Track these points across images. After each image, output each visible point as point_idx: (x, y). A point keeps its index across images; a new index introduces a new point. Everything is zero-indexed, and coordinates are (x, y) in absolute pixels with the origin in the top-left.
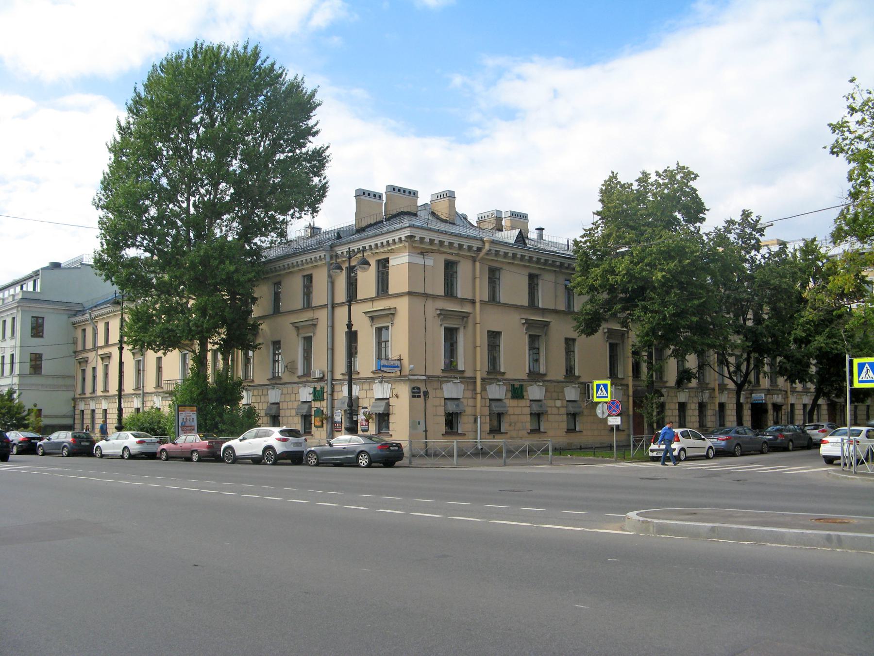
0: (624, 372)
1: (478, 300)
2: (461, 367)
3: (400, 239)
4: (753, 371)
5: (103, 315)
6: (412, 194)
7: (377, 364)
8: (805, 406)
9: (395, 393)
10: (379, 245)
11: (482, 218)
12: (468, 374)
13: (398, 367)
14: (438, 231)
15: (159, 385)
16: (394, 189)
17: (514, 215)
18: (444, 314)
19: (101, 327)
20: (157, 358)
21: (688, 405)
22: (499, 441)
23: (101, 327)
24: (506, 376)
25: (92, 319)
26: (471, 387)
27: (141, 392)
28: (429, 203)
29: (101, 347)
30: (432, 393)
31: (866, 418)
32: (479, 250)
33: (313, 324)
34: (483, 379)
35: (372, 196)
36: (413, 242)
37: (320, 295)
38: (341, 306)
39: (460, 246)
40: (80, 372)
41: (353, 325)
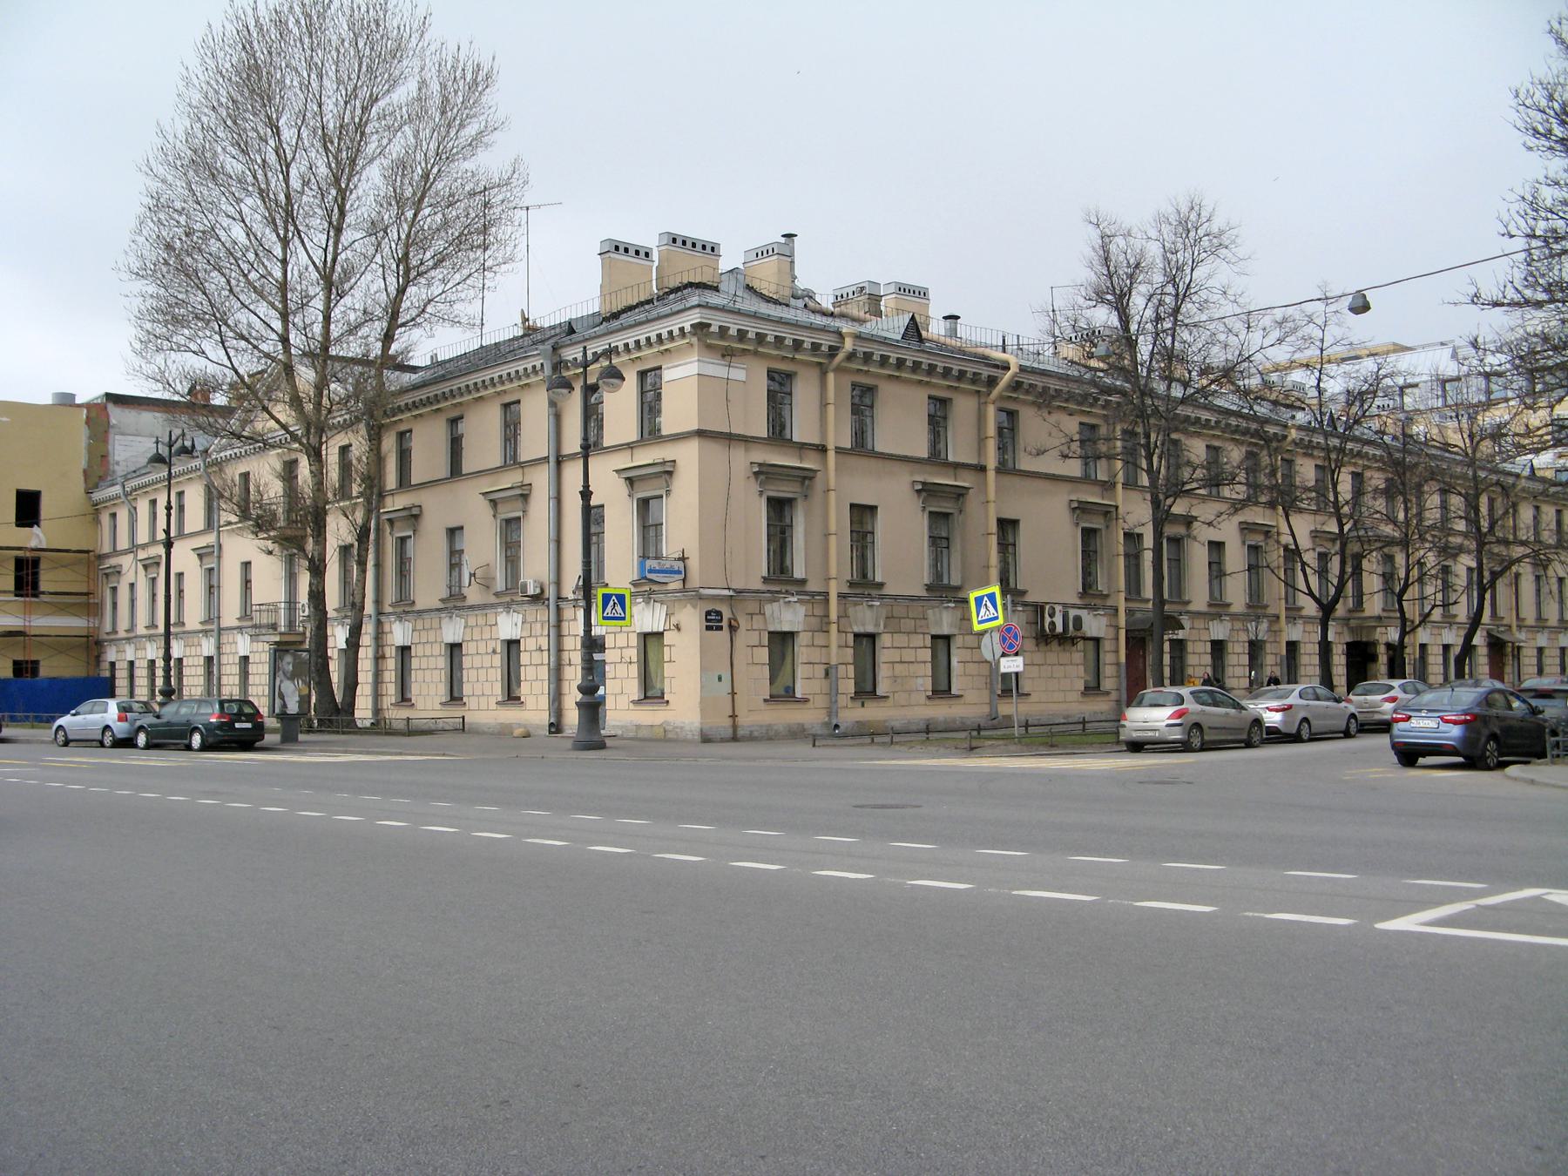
0: (1111, 578)
1: (831, 446)
2: (799, 573)
3: (682, 329)
4: (1350, 581)
5: (146, 486)
6: (708, 250)
7: (642, 566)
8: (1446, 648)
9: (674, 620)
10: (643, 342)
11: (842, 296)
12: (812, 586)
13: (679, 572)
14: (755, 316)
15: (246, 614)
16: (674, 240)
17: (903, 290)
18: (764, 473)
19: (143, 507)
20: (242, 563)
21: (1230, 645)
22: (871, 713)
23: (143, 507)
24: (886, 591)
25: (126, 495)
26: (818, 611)
27: (214, 627)
28: (741, 267)
29: (144, 546)
30: (743, 622)
31: (1559, 671)
32: (833, 351)
33: (522, 495)
34: (841, 596)
35: (631, 252)
36: (706, 335)
37: (534, 441)
38: (573, 459)
39: (798, 345)
40: (108, 593)
41: (592, 493)
